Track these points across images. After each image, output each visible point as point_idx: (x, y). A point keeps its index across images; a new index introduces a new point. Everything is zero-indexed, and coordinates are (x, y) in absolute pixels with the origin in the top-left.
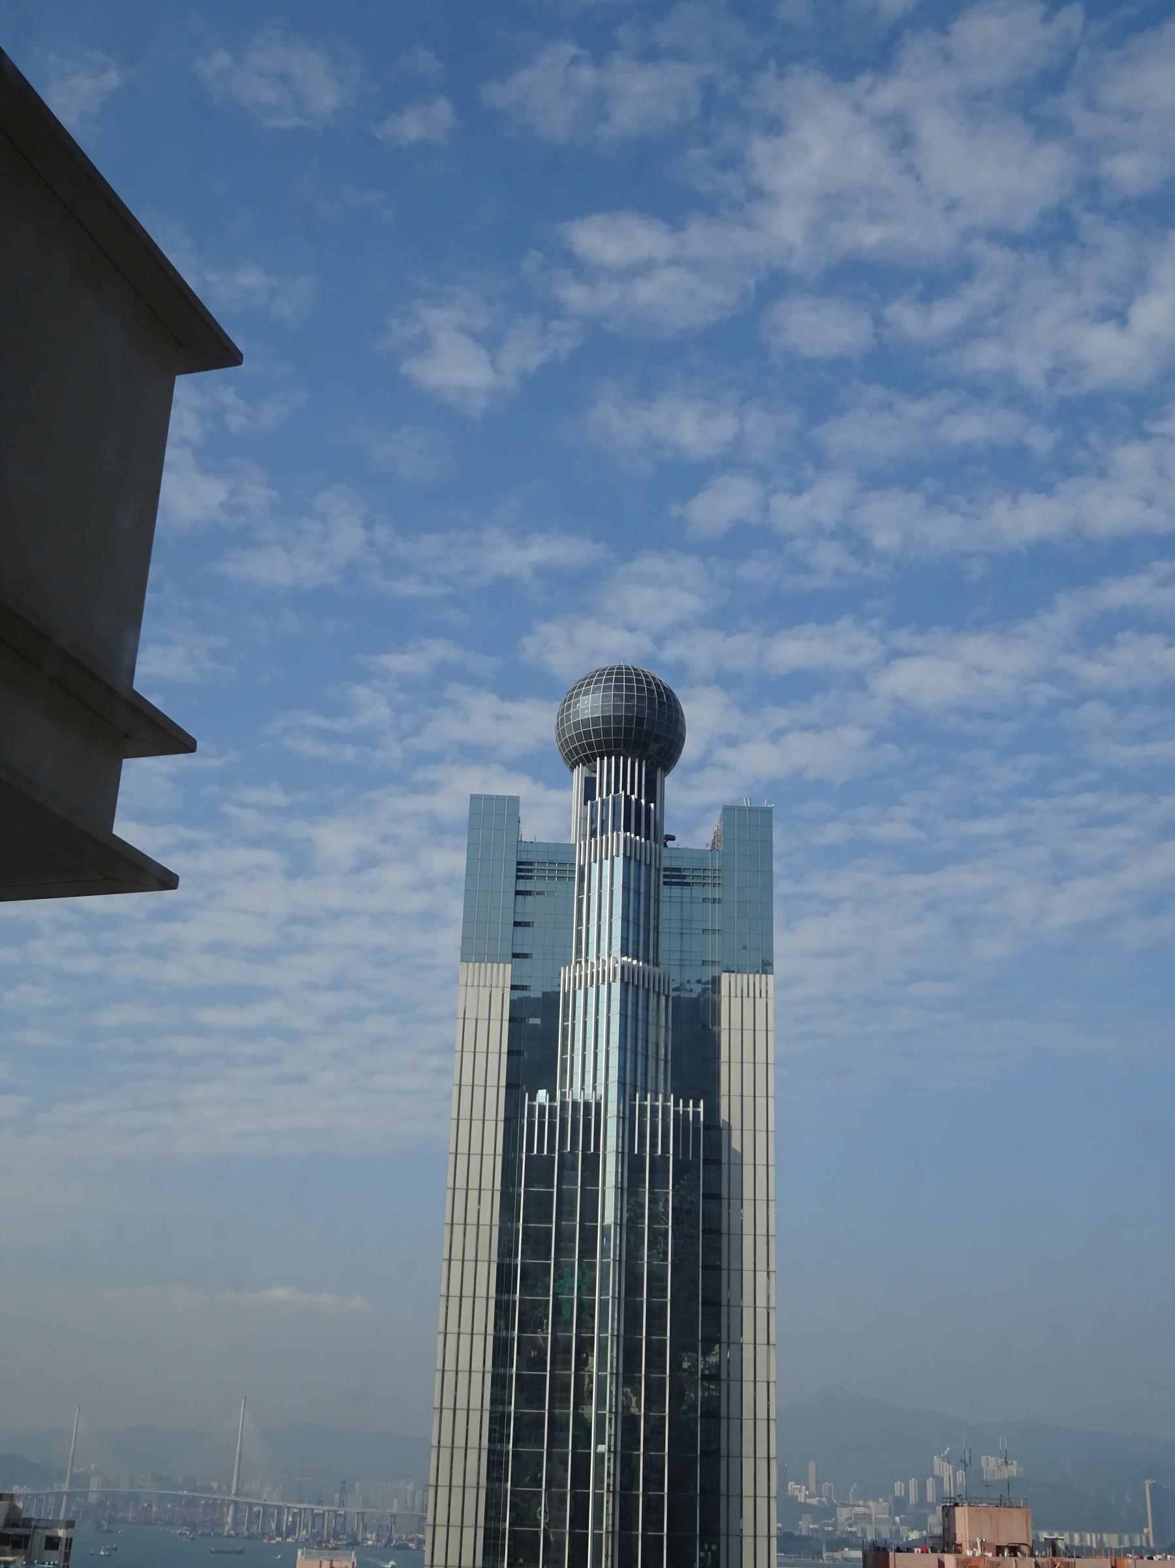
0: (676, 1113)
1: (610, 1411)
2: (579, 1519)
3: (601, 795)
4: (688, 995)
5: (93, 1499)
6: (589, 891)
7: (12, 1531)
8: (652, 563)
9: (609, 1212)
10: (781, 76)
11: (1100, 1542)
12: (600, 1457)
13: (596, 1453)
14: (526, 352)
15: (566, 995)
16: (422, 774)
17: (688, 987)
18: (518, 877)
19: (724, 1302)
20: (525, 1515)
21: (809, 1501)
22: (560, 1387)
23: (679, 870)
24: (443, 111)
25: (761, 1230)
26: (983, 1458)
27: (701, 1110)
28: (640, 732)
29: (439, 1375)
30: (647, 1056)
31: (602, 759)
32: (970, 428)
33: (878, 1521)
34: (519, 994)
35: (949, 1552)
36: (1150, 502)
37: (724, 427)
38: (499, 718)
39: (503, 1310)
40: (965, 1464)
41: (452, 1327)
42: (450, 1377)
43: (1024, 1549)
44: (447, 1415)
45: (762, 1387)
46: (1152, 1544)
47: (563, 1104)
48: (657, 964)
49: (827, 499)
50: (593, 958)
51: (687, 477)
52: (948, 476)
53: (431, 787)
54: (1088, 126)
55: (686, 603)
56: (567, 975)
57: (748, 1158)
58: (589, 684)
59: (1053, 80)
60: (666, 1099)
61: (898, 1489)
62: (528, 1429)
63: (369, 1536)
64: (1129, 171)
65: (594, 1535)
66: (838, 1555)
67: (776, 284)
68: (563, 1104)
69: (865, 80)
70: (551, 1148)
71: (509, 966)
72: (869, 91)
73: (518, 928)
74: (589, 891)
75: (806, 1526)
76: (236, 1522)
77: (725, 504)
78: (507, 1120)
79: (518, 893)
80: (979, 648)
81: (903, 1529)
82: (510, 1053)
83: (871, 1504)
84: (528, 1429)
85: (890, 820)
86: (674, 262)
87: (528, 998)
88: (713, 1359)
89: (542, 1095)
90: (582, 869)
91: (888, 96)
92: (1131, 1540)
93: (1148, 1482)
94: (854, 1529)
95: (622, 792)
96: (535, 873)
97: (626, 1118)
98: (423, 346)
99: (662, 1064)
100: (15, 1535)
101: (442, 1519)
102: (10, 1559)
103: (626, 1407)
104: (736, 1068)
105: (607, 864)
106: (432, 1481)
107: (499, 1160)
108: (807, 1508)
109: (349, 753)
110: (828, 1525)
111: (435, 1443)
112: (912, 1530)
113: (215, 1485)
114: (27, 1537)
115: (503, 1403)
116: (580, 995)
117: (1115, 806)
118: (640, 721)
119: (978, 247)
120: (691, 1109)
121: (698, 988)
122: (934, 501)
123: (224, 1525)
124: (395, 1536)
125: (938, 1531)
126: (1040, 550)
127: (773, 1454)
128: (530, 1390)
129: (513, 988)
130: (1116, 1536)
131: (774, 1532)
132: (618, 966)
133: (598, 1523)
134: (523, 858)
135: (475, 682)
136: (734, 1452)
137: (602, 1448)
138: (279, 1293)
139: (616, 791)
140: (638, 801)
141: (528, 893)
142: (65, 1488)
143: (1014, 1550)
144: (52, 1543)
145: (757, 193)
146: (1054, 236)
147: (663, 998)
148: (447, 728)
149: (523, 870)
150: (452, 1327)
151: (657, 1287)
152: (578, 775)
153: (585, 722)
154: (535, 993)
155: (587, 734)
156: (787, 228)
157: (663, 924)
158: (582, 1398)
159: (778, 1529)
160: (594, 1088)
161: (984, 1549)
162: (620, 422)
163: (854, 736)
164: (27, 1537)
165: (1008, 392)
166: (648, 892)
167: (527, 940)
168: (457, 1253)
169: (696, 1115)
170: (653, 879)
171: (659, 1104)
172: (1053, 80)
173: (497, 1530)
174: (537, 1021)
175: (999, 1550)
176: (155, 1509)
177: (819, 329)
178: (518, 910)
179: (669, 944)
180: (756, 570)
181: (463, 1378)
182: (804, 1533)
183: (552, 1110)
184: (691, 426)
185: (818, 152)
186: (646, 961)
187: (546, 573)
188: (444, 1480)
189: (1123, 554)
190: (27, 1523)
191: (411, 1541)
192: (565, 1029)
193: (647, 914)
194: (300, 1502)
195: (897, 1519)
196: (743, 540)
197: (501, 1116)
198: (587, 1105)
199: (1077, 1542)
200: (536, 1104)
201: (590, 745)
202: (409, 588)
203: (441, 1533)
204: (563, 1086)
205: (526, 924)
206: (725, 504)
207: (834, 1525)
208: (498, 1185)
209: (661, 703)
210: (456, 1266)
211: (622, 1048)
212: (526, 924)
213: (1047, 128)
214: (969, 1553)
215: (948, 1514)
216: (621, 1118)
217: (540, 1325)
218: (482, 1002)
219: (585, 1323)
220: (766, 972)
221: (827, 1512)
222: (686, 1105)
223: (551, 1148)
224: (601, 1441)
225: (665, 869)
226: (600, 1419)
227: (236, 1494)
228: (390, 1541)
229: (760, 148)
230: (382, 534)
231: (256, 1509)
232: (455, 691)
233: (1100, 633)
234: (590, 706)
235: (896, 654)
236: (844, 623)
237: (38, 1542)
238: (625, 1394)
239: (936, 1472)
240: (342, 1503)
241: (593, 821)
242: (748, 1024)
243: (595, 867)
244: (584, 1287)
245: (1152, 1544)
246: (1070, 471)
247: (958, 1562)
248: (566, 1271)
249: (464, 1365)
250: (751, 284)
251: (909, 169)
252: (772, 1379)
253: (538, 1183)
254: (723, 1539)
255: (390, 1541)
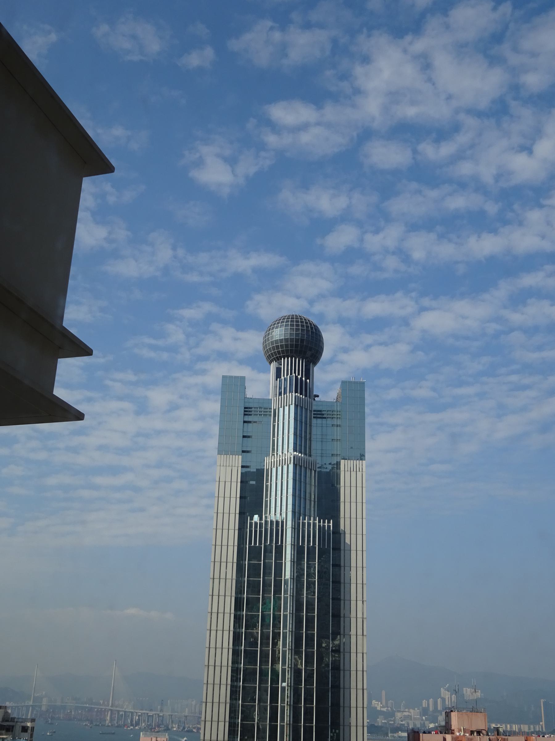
0: (319, 526)
1: (288, 667)
2: (274, 718)
3: (284, 376)
4: (325, 470)
5: (44, 708)
6: (278, 421)
7: (6, 724)
8: (308, 266)
9: (288, 573)
10: (369, 36)
11: (520, 729)
12: (283, 689)
13: (281, 687)
14: (248, 166)
15: (267, 470)
16: (199, 366)
17: (325, 466)
18: (245, 415)
19: (342, 615)
20: (248, 716)
21: (382, 709)
22: (265, 655)
23: (321, 411)
24: (209, 52)
25: (359, 581)
26: (464, 689)
27: (331, 524)
28: (302, 346)
29: (207, 650)
30: (305, 499)
31: (284, 359)
32: (458, 202)
33: (415, 719)
34: (245, 470)
35: (448, 733)
36: (543, 237)
37: (342, 202)
38: (236, 339)
39: (238, 619)
40: (456, 692)
41: (214, 627)
42: (212, 651)
43: (484, 732)
44: (211, 669)
45: (360, 656)
46: (544, 730)
47: (266, 522)
48: (310, 456)
49: (391, 236)
50: (280, 453)
51: (324, 225)
52: (448, 225)
53: (204, 372)
54: (514, 59)
55: (324, 285)
56: (268, 461)
57: (353, 547)
58: (278, 323)
59: (498, 38)
60: (315, 520)
61: (424, 703)
62: (250, 676)
63: (174, 726)
64: (533, 81)
65: (280, 725)
66: (396, 735)
67: (366, 134)
68: (266, 522)
69: (409, 38)
70: (260, 543)
71: (240, 457)
72: (411, 43)
73: (245, 439)
74: (278, 421)
75: (381, 721)
76: (112, 719)
77: (342, 238)
78: (239, 529)
79: (245, 422)
80: (462, 306)
81: (427, 722)
82: (241, 497)
83: (411, 711)
84: (250, 676)
85: (421, 387)
86: (318, 124)
87: (249, 472)
88: (337, 642)
89: (256, 518)
90: (275, 411)
91: (419, 45)
92: (534, 728)
93: (542, 701)
94: (403, 723)
95: (294, 374)
96: (253, 413)
97: (296, 528)
98: (200, 163)
99: (313, 503)
100: (7, 725)
101: (209, 718)
102: (5, 737)
103: (296, 665)
104: (348, 505)
105: (287, 408)
106: (204, 700)
107: (236, 548)
108: (381, 713)
109: (165, 356)
110: (391, 721)
111: (205, 682)
112: (431, 723)
113: (101, 702)
114: (13, 726)
115: (237, 663)
116: (274, 470)
117: (527, 381)
118: (302, 341)
119: (462, 117)
120: (326, 524)
121: (330, 467)
122: (441, 237)
123: (106, 721)
124: (187, 726)
125: (443, 723)
126: (491, 260)
127: (365, 687)
128: (251, 657)
129: (242, 467)
130: (527, 726)
131: (365, 724)
132: (292, 456)
133: (282, 720)
134: (247, 405)
135: (224, 322)
136: (347, 686)
137: (284, 684)
138: (132, 611)
139: (291, 374)
140: (301, 378)
141: (249, 422)
142: (31, 703)
143: (479, 733)
144: (25, 729)
145: (358, 91)
146: (498, 112)
147: (313, 472)
148: (211, 344)
149: (247, 411)
150: (214, 627)
151: (310, 608)
152: (273, 366)
153: (276, 341)
154: (253, 469)
155: (277, 347)
156: (372, 108)
157: (313, 437)
158: (275, 661)
159: (368, 722)
160: (281, 514)
161: (465, 732)
162: (293, 200)
163: (403, 348)
164: (13, 726)
165: (476, 185)
166: (306, 421)
167: (249, 444)
168: (216, 592)
169: (329, 527)
170: (308, 415)
171: (311, 522)
172: (498, 38)
173: (235, 723)
174: (254, 483)
175: (472, 733)
176: (73, 713)
177: (387, 155)
178: (245, 430)
179: (316, 446)
180: (357, 269)
181: (219, 651)
182: (380, 724)
183: (261, 524)
184: (326, 202)
185: (386, 72)
186: (305, 454)
187: (258, 271)
188: (210, 699)
189: (530, 262)
190: (13, 720)
191: (194, 728)
192: (267, 486)
193: (306, 432)
194: (142, 710)
195: (424, 718)
196: (351, 255)
197: (237, 527)
198: (277, 522)
199: (509, 729)
200: (253, 522)
201: (279, 352)
202: (193, 278)
203: (208, 724)
204: (266, 513)
205: (249, 437)
206: (342, 238)
207: (394, 721)
208: (235, 560)
209: (312, 332)
210: (215, 598)
211: (294, 495)
212: (249, 437)
213: (494, 61)
214: (458, 734)
215: (448, 715)
216: (293, 528)
217: (255, 626)
218: (228, 473)
219: (276, 625)
220: (362, 460)
221: (391, 714)
222: (324, 522)
223: (260, 543)
224: (284, 681)
225: (314, 411)
226: (284, 671)
227: (112, 706)
228: (184, 728)
229: (359, 70)
230: (181, 252)
231: (121, 713)
232: (215, 326)
233: (519, 299)
234: (279, 334)
235: (423, 309)
236: (399, 294)
237: (18, 729)
238: (295, 659)
239: (442, 696)
240: (161, 710)
241: (280, 388)
242: (353, 484)
243: (281, 410)
244: (276, 608)
245: (544, 730)
246: (506, 222)
247: (452, 738)
248: (267, 601)
249: (219, 645)
250: (355, 134)
251: (429, 80)
252: (365, 652)
253: (254, 559)
254: (341, 727)
255: (184, 728)
